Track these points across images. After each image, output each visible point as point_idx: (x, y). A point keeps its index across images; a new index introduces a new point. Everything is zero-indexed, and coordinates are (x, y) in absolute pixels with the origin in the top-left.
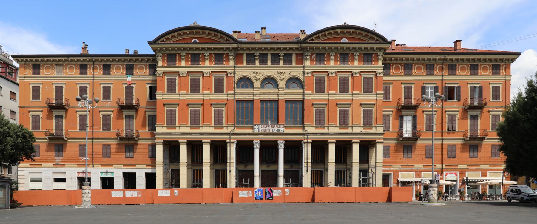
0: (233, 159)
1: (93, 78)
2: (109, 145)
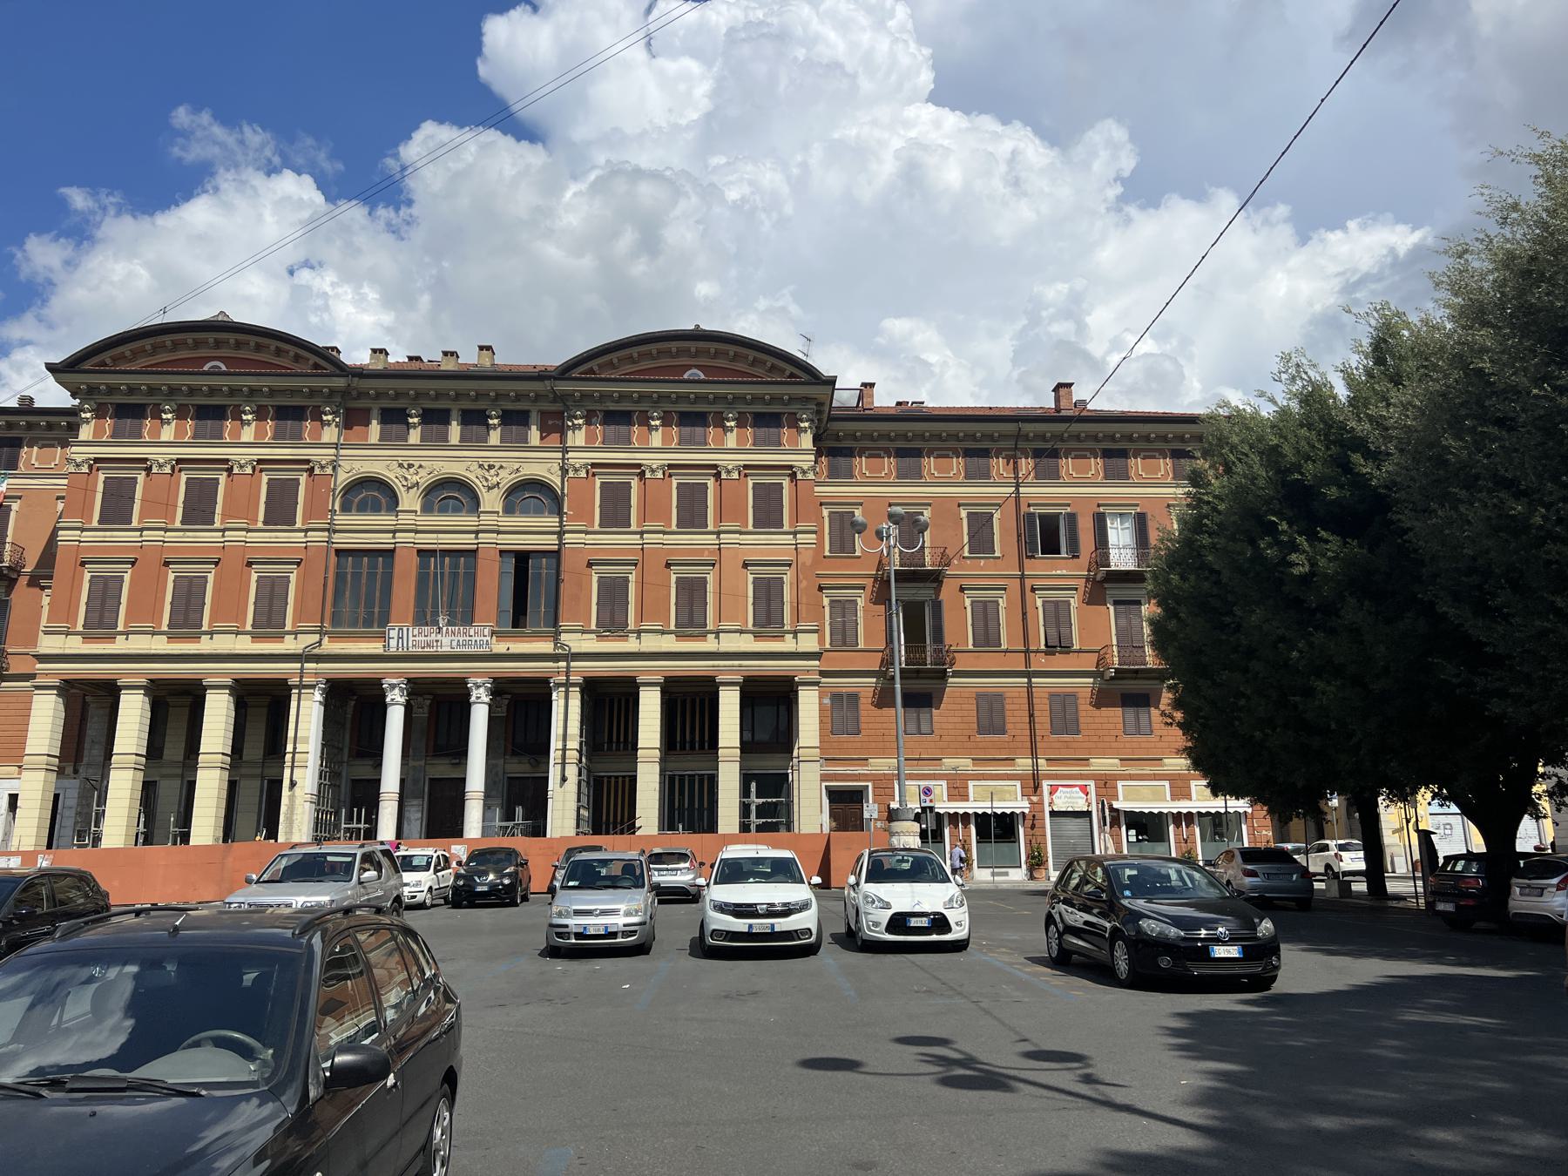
0: (308, 743)
2: (1074, 696)
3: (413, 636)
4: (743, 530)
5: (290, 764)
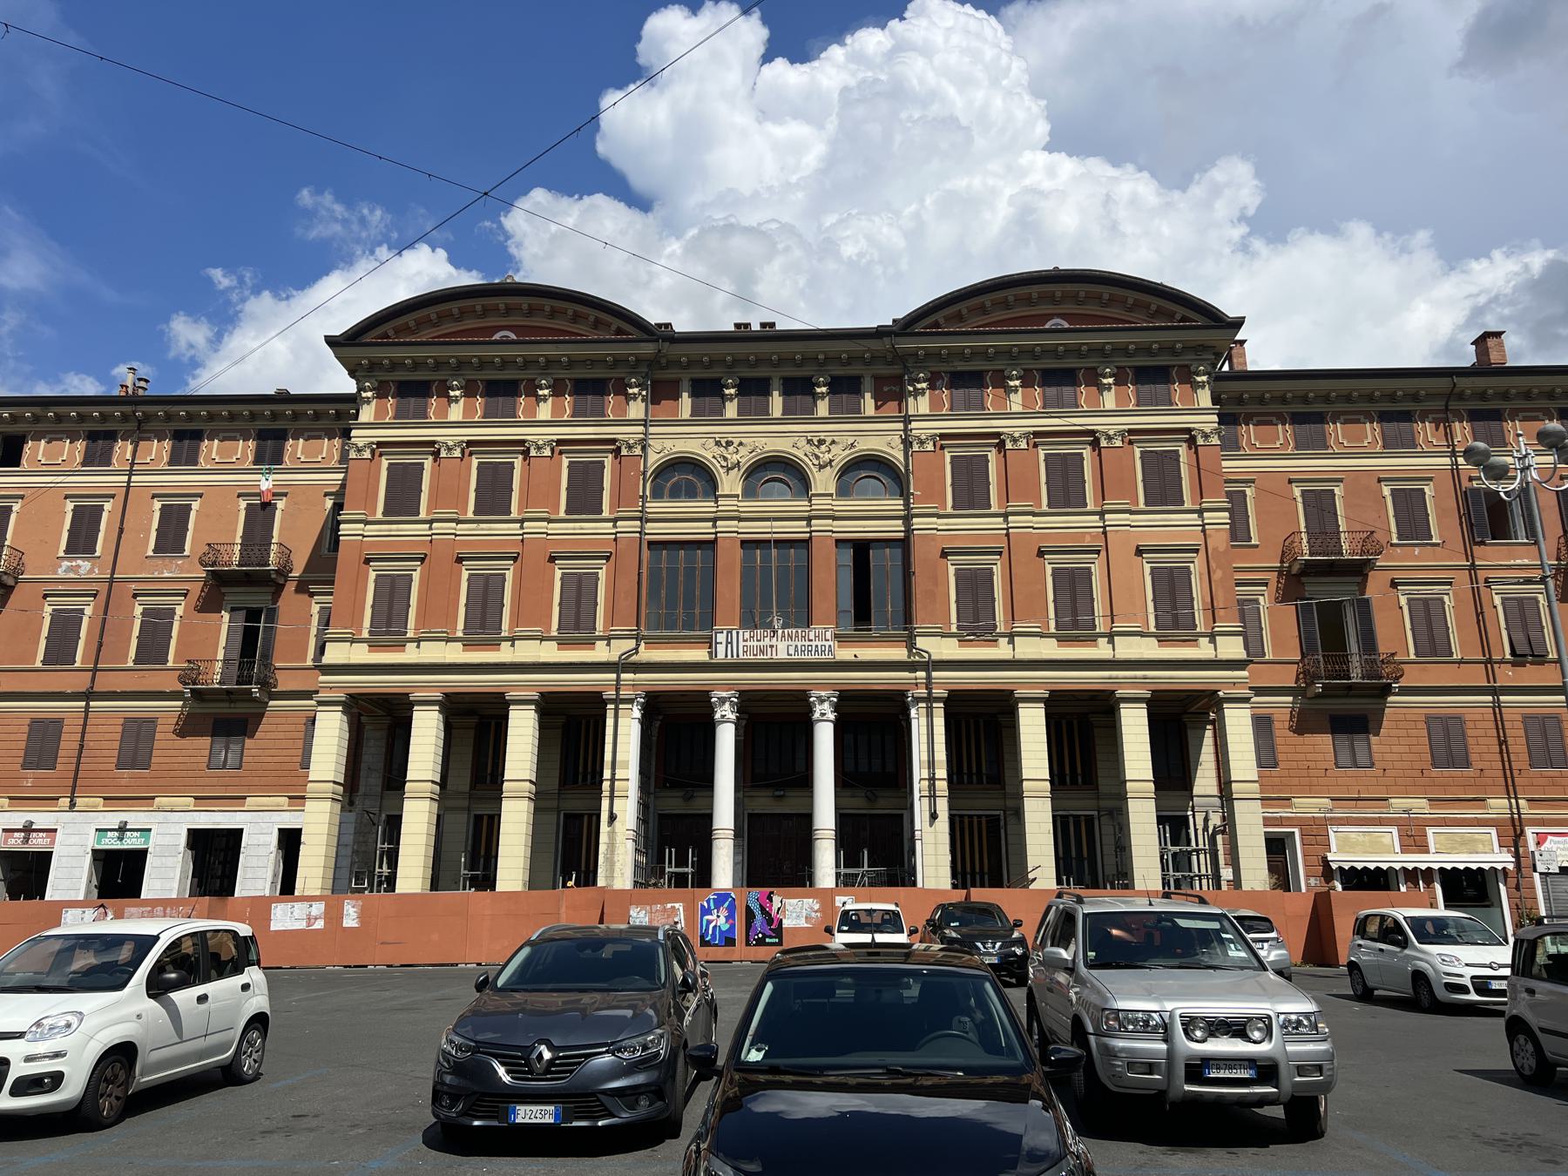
1: (130, 479)
3: (744, 641)
4: (1133, 508)
5: (607, 794)
